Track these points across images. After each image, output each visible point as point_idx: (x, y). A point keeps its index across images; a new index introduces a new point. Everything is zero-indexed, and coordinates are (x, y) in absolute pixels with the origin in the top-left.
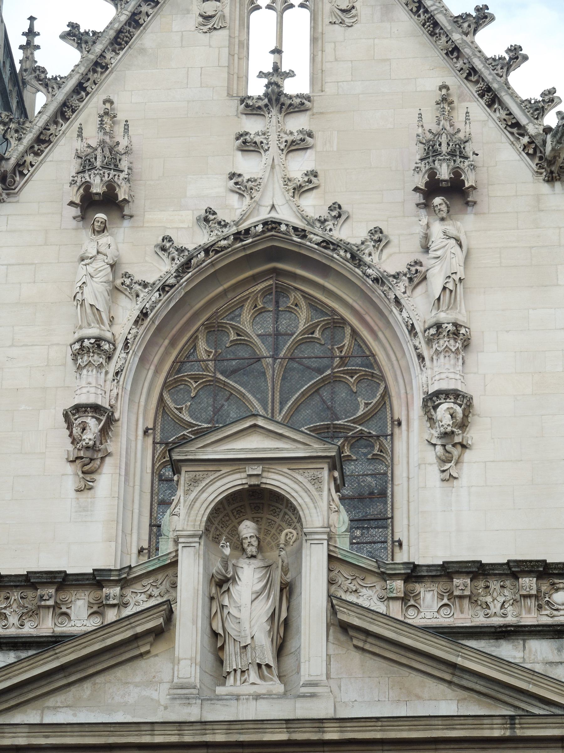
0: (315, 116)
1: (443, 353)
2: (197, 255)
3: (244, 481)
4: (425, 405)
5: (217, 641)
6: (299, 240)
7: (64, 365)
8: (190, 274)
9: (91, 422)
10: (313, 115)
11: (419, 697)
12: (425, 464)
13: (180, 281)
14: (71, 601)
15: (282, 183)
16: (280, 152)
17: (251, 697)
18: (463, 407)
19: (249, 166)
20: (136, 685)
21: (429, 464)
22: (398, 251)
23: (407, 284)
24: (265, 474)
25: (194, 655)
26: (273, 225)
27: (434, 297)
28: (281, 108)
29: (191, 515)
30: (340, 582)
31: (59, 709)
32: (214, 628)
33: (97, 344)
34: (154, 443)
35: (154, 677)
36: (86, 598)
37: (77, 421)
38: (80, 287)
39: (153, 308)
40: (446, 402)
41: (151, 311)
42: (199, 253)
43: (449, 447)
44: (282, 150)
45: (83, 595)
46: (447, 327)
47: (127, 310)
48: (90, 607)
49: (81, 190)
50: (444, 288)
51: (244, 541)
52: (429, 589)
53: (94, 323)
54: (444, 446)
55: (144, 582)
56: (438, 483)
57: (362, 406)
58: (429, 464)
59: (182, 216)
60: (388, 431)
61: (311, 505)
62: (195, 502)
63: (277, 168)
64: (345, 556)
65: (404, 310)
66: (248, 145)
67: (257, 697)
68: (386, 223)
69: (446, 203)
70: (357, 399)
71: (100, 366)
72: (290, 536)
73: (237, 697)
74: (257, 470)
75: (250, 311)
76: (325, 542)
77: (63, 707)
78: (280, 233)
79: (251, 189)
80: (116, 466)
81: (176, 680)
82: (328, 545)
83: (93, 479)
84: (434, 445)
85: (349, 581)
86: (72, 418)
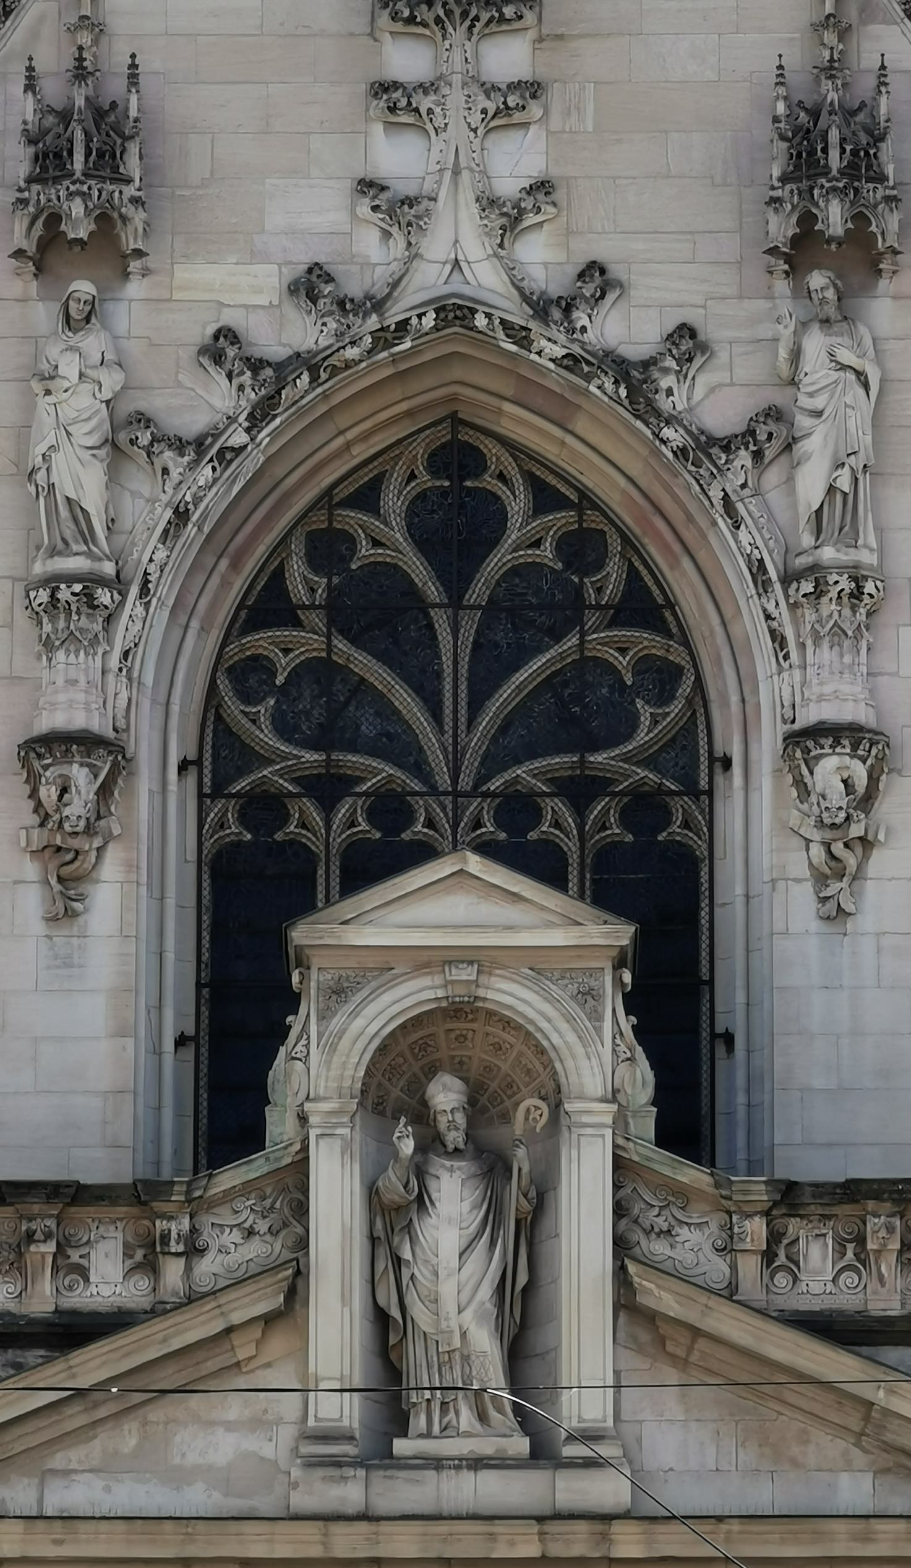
0: (544, 45)
1: (827, 639)
2: (294, 380)
3: (440, 993)
4: (787, 755)
5: (387, 1330)
6: (513, 348)
7: (10, 626)
8: (278, 421)
9: (79, 775)
10: (540, 40)
11: (795, 1463)
12: (787, 879)
13: (256, 437)
14: (89, 1241)
15: (475, 208)
16: (472, 134)
17: (464, 1462)
18: (869, 762)
19: (399, 158)
20: (229, 1426)
21: (794, 880)
22: (728, 381)
23: (749, 463)
24: (483, 979)
25: (347, 1372)
26: (458, 313)
27: (810, 507)
28: (472, 27)
29: (334, 1066)
30: (636, 1211)
31: (74, 1477)
32: (382, 1302)
33: (85, 595)
34: (201, 796)
35: (266, 1411)
36: (120, 1236)
37: (48, 774)
38: (43, 455)
39: (197, 500)
40: (834, 753)
41: (196, 506)
42: (299, 377)
43: (838, 848)
44: (475, 130)
45: (112, 1228)
46: (837, 582)
47: (145, 504)
48: (128, 1254)
49: (40, 223)
50: (831, 490)
51: (439, 1117)
52: (817, 1232)
53: (77, 542)
54: (827, 846)
55: (239, 1205)
56: (815, 925)
57: (645, 721)
58: (794, 880)
59: (256, 276)
60: (702, 783)
61: (579, 1050)
62: (340, 1038)
63: (465, 175)
64: (649, 1159)
65: (743, 527)
66: (394, 100)
67: (477, 1463)
68: (702, 311)
69: (835, 286)
70: (633, 702)
71: (95, 641)
72: (535, 1114)
73: (437, 1463)
74: (467, 974)
75: (400, 492)
76: (609, 1133)
77: (84, 1471)
78: (471, 329)
79: (409, 224)
80: (131, 866)
81: (311, 1422)
82: (614, 1133)
83: (82, 895)
84: (808, 841)
85: (656, 1211)
86: (36, 764)
